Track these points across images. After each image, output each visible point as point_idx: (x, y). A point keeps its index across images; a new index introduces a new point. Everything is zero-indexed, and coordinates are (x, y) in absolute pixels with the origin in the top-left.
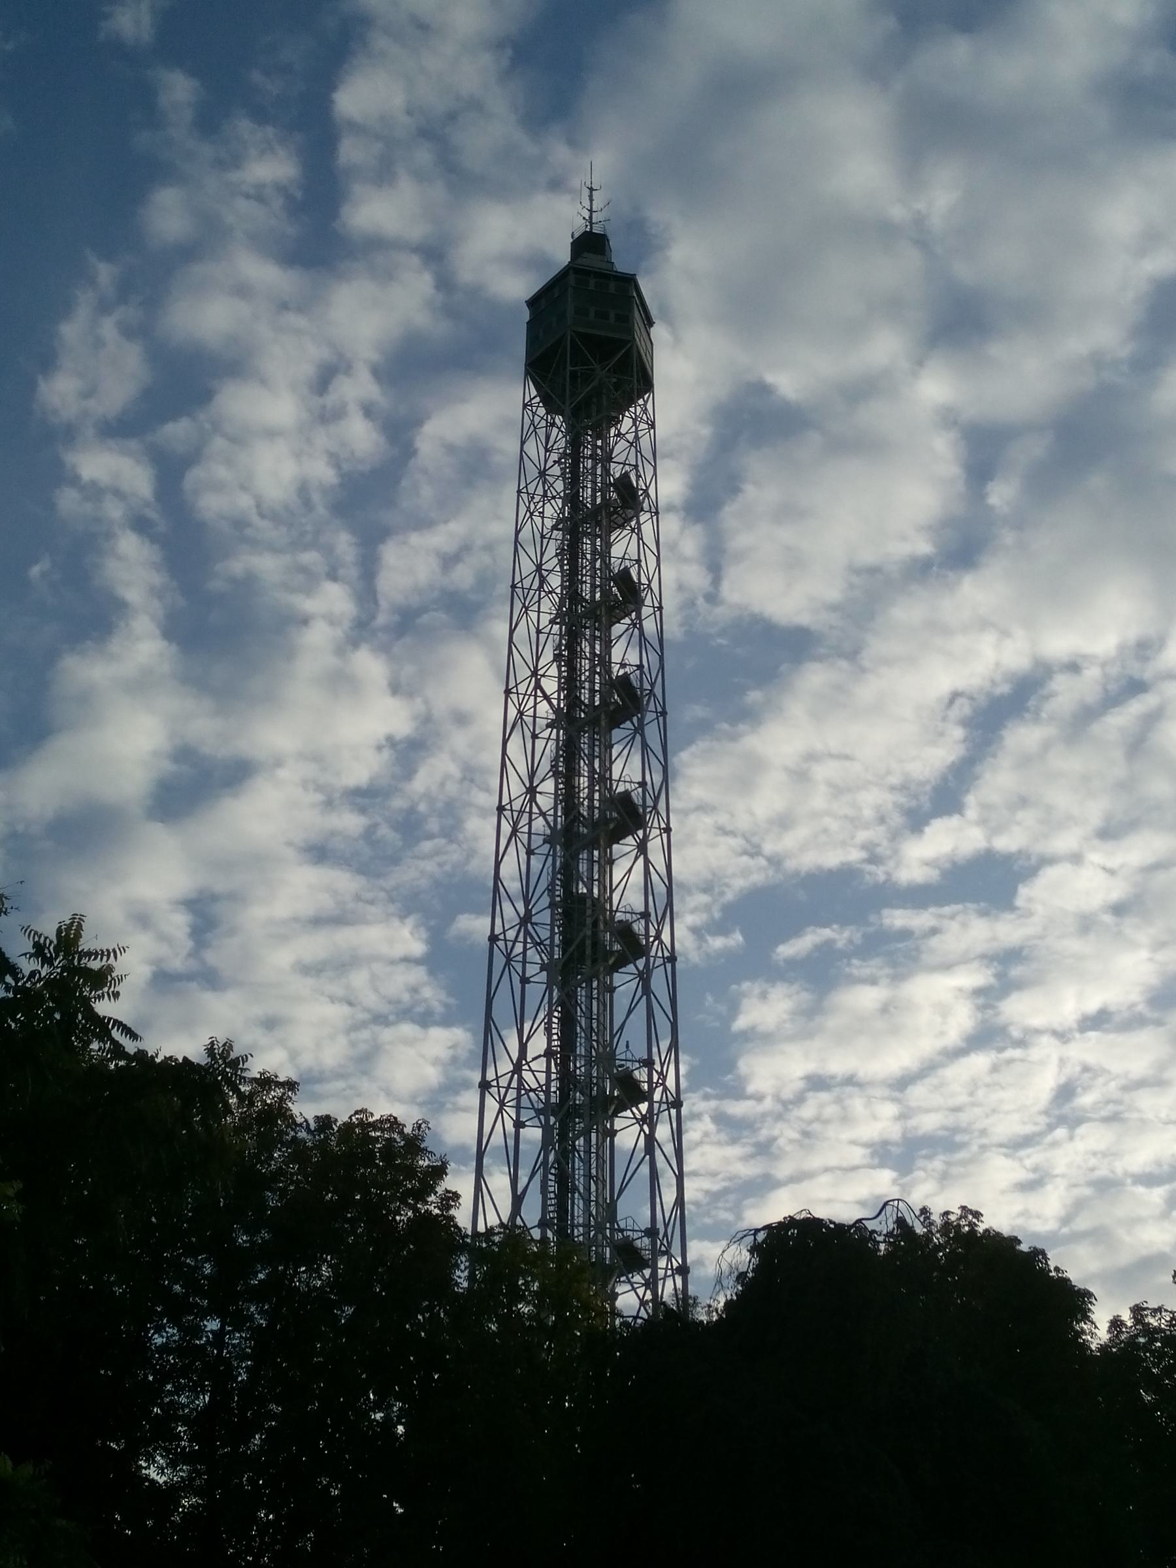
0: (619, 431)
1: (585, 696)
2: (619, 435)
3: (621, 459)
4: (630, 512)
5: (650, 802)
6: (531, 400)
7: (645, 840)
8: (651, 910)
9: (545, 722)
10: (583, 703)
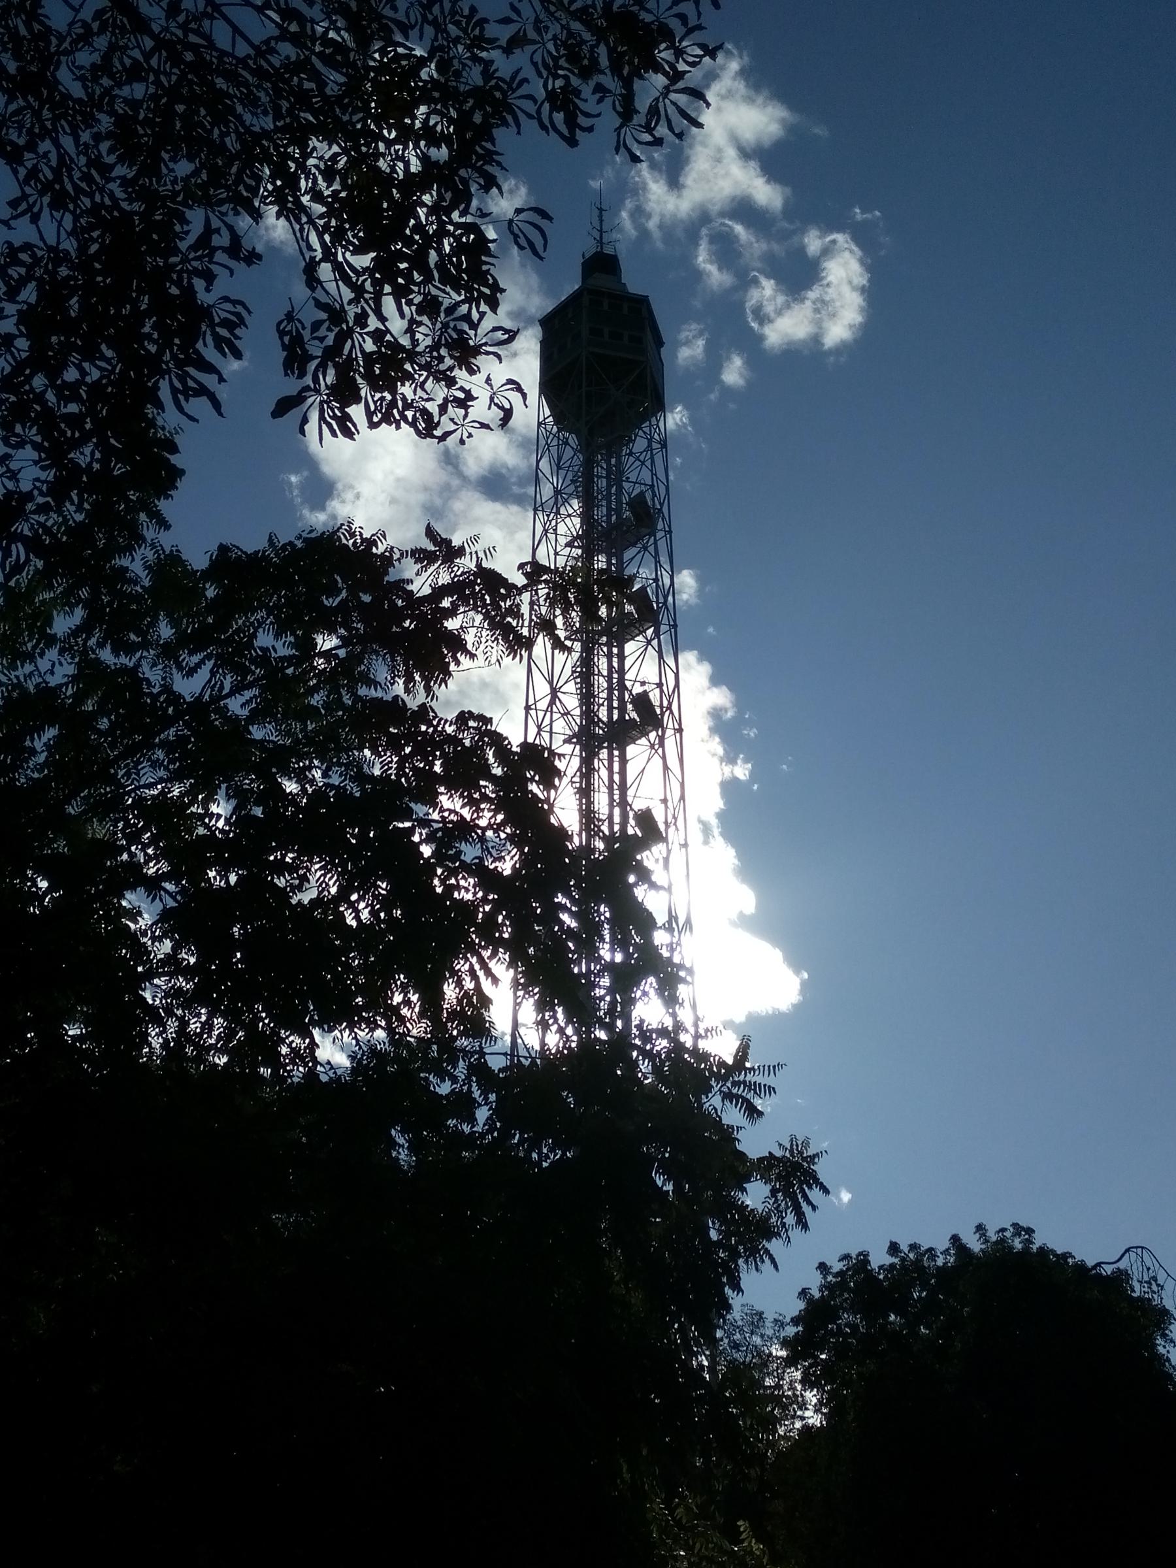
0: (631, 450)
1: (603, 714)
2: (631, 454)
3: (633, 478)
4: (644, 530)
5: (665, 703)
6: (545, 419)
7: (662, 739)
8: (669, 797)
9: (563, 737)
10: (600, 720)
